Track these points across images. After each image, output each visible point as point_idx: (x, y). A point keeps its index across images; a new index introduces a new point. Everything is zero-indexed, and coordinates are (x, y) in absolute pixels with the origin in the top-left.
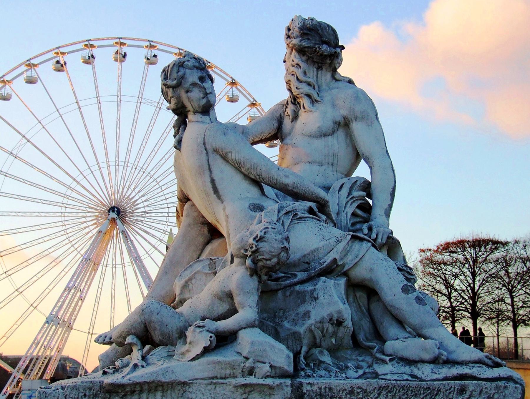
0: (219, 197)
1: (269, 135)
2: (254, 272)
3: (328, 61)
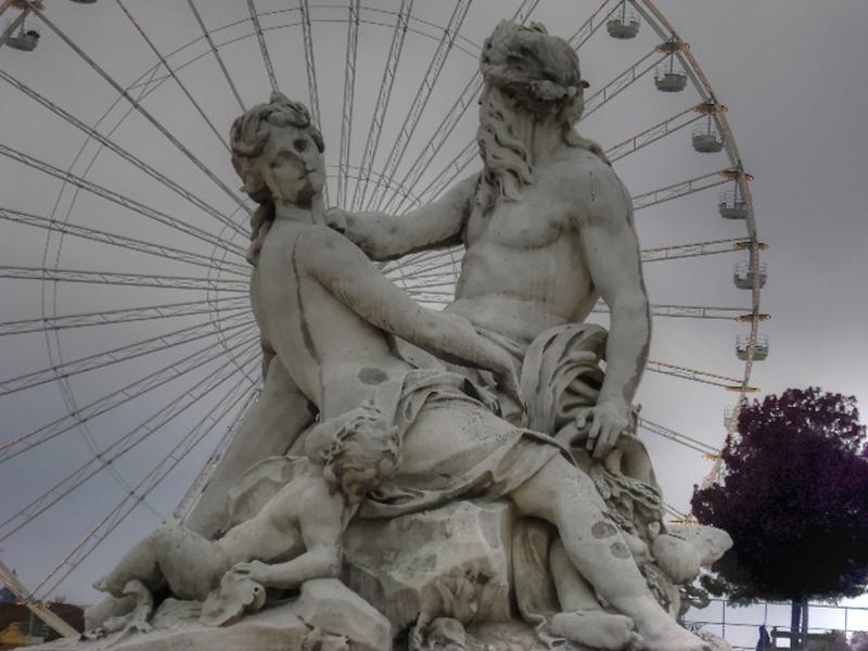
0: (314, 354)
1: (446, 237)
2: (336, 488)
3: (554, 110)
